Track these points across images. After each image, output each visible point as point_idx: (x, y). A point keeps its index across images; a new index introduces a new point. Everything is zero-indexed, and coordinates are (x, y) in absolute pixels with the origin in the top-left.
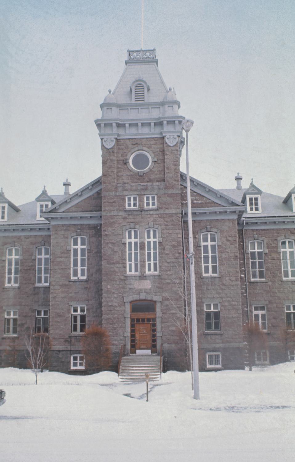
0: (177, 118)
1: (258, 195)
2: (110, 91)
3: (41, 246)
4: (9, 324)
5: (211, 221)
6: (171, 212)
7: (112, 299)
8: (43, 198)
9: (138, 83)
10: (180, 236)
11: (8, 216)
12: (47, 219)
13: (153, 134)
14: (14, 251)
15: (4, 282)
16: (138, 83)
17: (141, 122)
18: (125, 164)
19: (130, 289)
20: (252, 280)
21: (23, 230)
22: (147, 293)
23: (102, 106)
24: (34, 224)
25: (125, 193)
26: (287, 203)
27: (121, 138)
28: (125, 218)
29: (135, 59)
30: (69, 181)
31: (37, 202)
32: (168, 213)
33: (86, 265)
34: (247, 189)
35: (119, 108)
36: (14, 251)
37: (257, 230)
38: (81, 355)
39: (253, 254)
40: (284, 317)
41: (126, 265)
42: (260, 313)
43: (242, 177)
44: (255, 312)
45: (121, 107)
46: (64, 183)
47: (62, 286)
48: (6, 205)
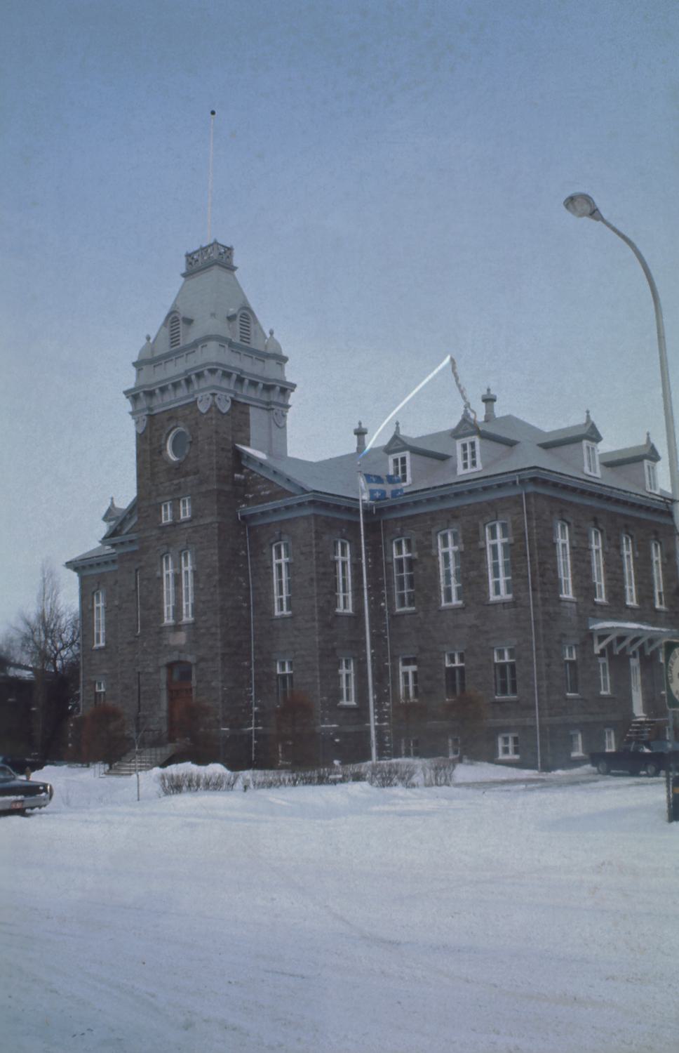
0: (205, 367)
1: (473, 437)
2: (148, 338)
3: (444, 529)
4: (454, 678)
5: (282, 522)
6: (206, 522)
7: (148, 662)
8: (396, 446)
9: (170, 318)
10: (215, 558)
11: (413, 477)
12: (114, 546)
13: (181, 399)
14: (450, 538)
15: (486, 593)
16: (170, 318)
17: (142, 390)
18: (160, 452)
19: (166, 645)
20: (398, 610)
21: (499, 486)
22: (181, 652)
23: (138, 365)
24: (491, 476)
25: (159, 500)
26: (513, 447)
27: (155, 412)
28: (159, 539)
29: (211, 261)
30: (363, 426)
31: (386, 455)
32: (202, 523)
33: (395, 578)
34: (386, 446)
35: (152, 365)
36: (450, 538)
37: (402, 518)
38: (516, 735)
39: (400, 561)
40: (443, 676)
41: (570, 551)
42: (411, 669)
43: (496, 396)
44: (402, 669)
45: (166, 358)
46: (483, 396)
47: (130, 643)
48: (407, 454)
